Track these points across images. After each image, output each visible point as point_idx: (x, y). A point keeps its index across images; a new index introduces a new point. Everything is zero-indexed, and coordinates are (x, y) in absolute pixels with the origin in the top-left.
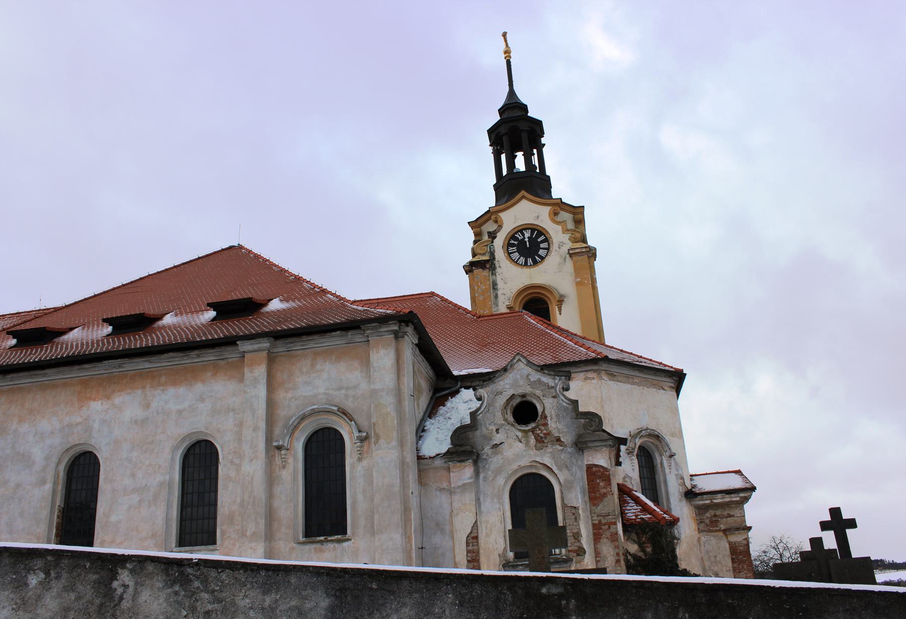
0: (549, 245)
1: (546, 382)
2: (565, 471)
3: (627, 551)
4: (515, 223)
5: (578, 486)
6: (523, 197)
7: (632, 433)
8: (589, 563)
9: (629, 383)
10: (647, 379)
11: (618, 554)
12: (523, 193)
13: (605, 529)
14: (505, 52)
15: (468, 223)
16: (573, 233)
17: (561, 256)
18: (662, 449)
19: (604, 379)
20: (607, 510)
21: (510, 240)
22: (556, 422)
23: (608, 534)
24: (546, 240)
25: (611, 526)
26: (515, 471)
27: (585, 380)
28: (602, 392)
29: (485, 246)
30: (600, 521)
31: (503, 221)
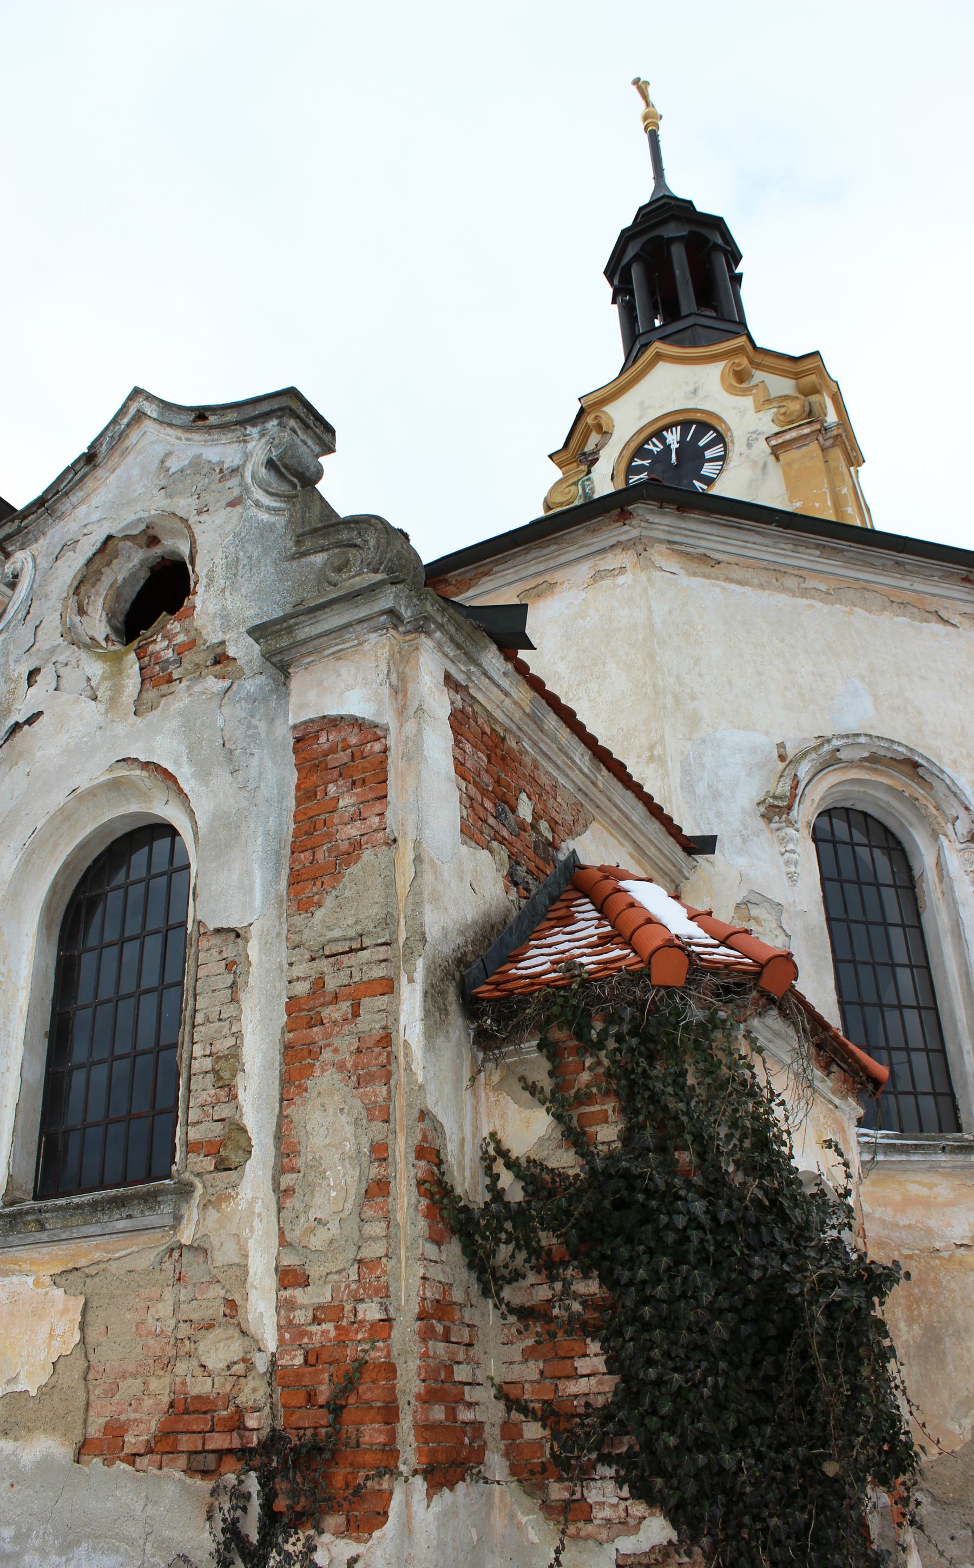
0: (725, 450)
1: (215, 459)
2: (222, 777)
3: (498, 1143)
4: (640, 418)
5: (260, 831)
6: (659, 357)
7: (791, 752)
8: (258, 1208)
9: (784, 589)
10: (868, 586)
11: (380, 1153)
12: (658, 346)
13: (335, 1022)
14: (645, 118)
15: (551, 456)
16: (784, 404)
17: (755, 464)
18: (934, 811)
19: (661, 569)
20: (350, 921)
21: (632, 460)
22: (223, 590)
23: (345, 1044)
24: (720, 439)
25: (366, 1002)
26: (64, 817)
27: (595, 581)
28: (649, 608)
29: (572, 485)
30: (319, 983)
31: (612, 421)
